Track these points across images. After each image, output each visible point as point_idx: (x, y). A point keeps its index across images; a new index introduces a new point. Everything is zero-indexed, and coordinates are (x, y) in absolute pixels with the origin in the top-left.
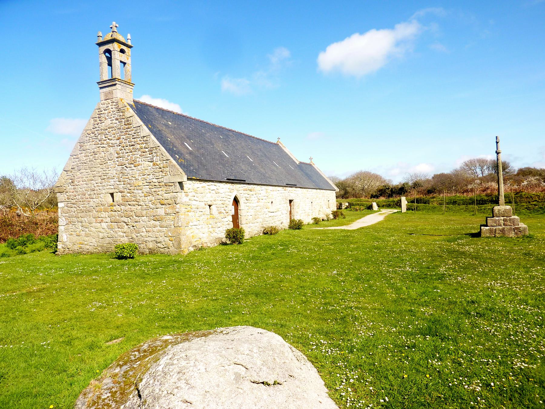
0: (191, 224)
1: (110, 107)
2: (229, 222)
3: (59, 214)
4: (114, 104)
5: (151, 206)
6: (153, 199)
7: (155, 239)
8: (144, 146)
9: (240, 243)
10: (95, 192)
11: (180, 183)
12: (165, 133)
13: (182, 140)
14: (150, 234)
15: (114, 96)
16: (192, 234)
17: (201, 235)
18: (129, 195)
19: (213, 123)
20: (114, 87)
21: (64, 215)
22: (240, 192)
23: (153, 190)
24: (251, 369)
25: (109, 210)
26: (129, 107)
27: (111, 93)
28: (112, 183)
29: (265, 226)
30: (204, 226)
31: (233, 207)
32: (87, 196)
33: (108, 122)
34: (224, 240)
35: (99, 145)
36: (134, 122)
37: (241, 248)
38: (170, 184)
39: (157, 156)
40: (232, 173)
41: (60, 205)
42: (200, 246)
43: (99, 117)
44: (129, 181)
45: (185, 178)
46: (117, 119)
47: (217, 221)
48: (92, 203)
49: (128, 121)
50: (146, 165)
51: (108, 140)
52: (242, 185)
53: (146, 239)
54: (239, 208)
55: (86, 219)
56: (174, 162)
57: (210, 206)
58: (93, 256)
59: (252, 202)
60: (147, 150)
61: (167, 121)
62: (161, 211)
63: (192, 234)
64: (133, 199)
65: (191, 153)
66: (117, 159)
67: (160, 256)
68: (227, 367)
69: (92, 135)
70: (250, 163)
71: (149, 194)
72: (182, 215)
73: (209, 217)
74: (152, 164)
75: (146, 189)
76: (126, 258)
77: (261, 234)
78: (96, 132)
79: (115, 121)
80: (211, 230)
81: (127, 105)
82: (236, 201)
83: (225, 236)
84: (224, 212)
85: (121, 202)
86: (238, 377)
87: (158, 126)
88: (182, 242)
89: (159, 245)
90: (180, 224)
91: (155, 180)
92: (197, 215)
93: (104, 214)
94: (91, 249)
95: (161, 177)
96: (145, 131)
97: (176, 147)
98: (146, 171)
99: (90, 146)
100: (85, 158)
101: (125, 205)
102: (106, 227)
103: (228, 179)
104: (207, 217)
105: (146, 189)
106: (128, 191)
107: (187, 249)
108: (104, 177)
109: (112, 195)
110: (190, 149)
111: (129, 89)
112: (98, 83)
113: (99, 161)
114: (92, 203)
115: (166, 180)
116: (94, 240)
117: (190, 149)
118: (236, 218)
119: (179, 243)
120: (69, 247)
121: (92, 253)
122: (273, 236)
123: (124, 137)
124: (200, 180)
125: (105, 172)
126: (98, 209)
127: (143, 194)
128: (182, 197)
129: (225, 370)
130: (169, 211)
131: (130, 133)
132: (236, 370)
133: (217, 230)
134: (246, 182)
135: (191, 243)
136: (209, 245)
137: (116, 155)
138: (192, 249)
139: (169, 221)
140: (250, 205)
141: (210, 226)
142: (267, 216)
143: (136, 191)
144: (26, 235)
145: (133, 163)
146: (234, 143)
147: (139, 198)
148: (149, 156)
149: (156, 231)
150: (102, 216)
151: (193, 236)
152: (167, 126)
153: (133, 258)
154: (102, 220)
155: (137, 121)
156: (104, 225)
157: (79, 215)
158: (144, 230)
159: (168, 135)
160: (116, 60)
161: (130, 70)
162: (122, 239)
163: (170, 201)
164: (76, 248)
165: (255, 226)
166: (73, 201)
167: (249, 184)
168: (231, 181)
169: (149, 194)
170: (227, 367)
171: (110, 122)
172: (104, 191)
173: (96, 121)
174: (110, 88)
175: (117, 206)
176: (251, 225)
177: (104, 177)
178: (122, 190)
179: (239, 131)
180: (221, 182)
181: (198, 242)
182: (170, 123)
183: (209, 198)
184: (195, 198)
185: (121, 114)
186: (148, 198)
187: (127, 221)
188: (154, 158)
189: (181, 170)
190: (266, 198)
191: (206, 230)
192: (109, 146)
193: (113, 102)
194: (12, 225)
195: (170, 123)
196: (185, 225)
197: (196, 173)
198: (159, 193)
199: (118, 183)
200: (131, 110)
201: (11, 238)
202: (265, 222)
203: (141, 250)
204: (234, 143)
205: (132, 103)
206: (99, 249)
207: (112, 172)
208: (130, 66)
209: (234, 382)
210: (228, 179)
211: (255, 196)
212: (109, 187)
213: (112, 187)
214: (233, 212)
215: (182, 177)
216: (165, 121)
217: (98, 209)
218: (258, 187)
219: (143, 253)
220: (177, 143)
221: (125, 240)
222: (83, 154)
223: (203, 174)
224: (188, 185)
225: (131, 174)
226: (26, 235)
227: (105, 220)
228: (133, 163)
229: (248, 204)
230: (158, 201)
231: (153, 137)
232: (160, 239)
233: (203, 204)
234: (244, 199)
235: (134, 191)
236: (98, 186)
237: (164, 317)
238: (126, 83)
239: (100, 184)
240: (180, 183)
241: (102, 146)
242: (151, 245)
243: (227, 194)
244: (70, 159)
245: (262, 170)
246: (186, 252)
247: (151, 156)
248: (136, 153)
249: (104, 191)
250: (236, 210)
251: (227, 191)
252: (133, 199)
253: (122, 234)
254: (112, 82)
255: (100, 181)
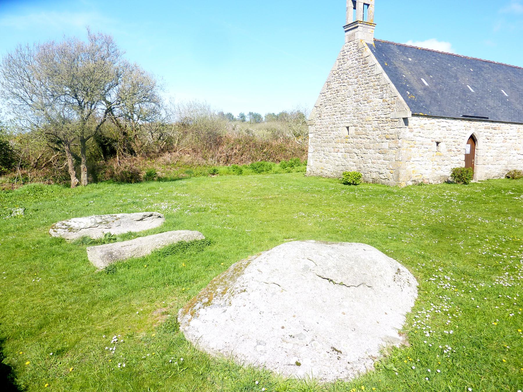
0: (413, 159)
1: (352, 49)
2: (460, 161)
3: (309, 143)
4: (356, 45)
5: (378, 140)
6: (380, 133)
7: (378, 170)
8: (376, 83)
9: (465, 183)
10: (335, 125)
11: (406, 120)
12: (402, 70)
13: (420, 75)
14: (375, 166)
15: (356, 38)
16: (413, 169)
17: (423, 171)
18: (360, 129)
19: (465, 55)
20: (356, 30)
21: (312, 144)
22: (480, 130)
23: (380, 125)
24: (319, 266)
25: (345, 141)
26: (367, 47)
27: (353, 35)
28: (349, 117)
29: (510, 169)
30: (427, 163)
31: (469, 145)
32: (329, 129)
33: (350, 62)
34: (450, 179)
35: (341, 84)
36: (370, 61)
37: (465, 189)
38: (396, 120)
39: (387, 93)
40: (472, 110)
41: (310, 136)
42: (420, 181)
43: (343, 59)
44: (362, 117)
45: (409, 114)
46: (357, 60)
47: (445, 159)
48: (332, 135)
49: (365, 60)
50: (376, 101)
51: (348, 79)
52: (483, 123)
53: (371, 169)
54: (476, 147)
55: (327, 148)
56: (401, 98)
57: (438, 143)
58: (330, 180)
59: (495, 141)
60: (379, 87)
61: (408, 57)
62: (385, 145)
63: (413, 169)
64: (364, 132)
65: (425, 89)
66: (354, 96)
67: (380, 186)
68: (301, 260)
69: (337, 75)
70: (502, 99)
71: (377, 128)
72: (404, 150)
73: (435, 154)
74: (382, 100)
75: (375, 124)
76: (349, 184)
77: (503, 178)
78: (340, 72)
79: (355, 61)
80: (436, 167)
81: (365, 45)
82: (473, 139)
83: (450, 174)
84: (455, 150)
85: (354, 135)
86: (306, 268)
87: (395, 63)
88: (400, 175)
89: (381, 176)
90: (400, 159)
91: (383, 116)
92: (421, 151)
93: (340, 145)
94: (329, 174)
95: (388, 113)
96: (379, 68)
97: (409, 83)
98: (376, 107)
99: (335, 85)
100: (330, 96)
101: (357, 138)
102: (340, 156)
103: (464, 116)
104: (432, 154)
105: (375, 124)
106: (361, 125)
107: (405, 182)
108: (343, 112)
109: (348, 128)
110: (426, 84)
111: (370, 29)
112: (344, 27)
113: (340, 98)
114: (332, 135)
115: (391, 116)
116: (331, 167)
117: (426, 84)
118: (470, 159)
119: (398, 176)
120: (314, 170)
121: (329, 178)
122: (514, 180)
123: (361, 75)
124: (428, 116)
125: (343, 108)
126: (336, 140)
127: (372, 129)
128: (405, 132)
129: (299, 261)
130: (392, 145)
131: (366, 71)
132: (307, 264)
133: (443, 168)
134: (489, 120)
135: (410, 177)
136: (431, 181)
137: (354, 92)
138: (410, 183)
139: (391, 154)
140: (492, 145)
141: (435, 163)
142: (515, 158)
143: (366, 126)
144: (295, 158)
145: (367, 100)
146: (487, 76)
147: (368, 132)
148: (380, 93)
149: (379, 163)
150: (339, 146)
151: (413, 171)
152: (406, 62)
153: (356, 185)
154: (338, 150)
155: (373, 60)
156: (340, 154)
157: (323, 144)
158: (370, 162)
159: (405, 72)
160: (360, 3)
161: (373, 11)
162: (352, 168)
163: (393, 136)
164: (318, 171)
165: (496, 168)
166: (319, 133)
167: (492, 122)
168: (467, 118)
169: (377, 128)
170: (301, 260)
171: (351, 62)
172: (342, 125)
173: (340, 62)
174: (351, 32)
175: (351, 139)
176: (490, 166)
177: (343, 112)
178: (356, 124)
179: (500, 62)
180: (455, 119)
181: (419, 178)
182: (410, 59)
183: (437, 135)
184: (421, 134)
185: (360, 54)
186: (376, 132)
187: (357, 152)
188: (384, 95)
189: (406, 106)
190: (516, 138)
191: (431, 167)
192: (349, 85)
193: (355, 44)
194: (286, 150)
195: (410, 59)
196: (406, 159)
197: (425, 109)
198: (385, 128)
199: (353, 118)
200: (369, 50)
201: (283, 160)
202: (511, 165)
203: (366, 179)
204: (487, 76)
205: (373, 43)
206: (335, 174)
207: (350, 108)
208: (373, 6)
209: (301, 270)
210: (464, 116)
211: (500, 135)
212: (346, 121)
213: (348, 121)
214: (468, 151)
215: (406, 114)
216: (405, 58)
217: (336, 140)
218: (507, 126)
219: (367, 182)
220: (413, 80)
221: (353, 169)
222: (329, 93)
223: (434, 110)
224: (413, 121)
225: (364, 110)
226: (295, 158)
227: (340, 150)
228: (367, 100)
229: (488, 144)
230: (384, 135)
231: (385, 75)
232: (382, 171)
233: (430, 140)
234: (484, 138)
235: (365, 126)
236: (338, 120)
237: (338, 232)
238: (368, 24)
239: (339, 119)
240: (406, 120)
241: (343, 84)
242: (374, 176)
243: (462, 131)
244: (320, 97)
245: (518, 106)
246: (403, 185)
247: (381, 93)
248: (369, 90)
249: (342, 125)
250: (473, 149)
251: (464, 129)
252: (364, 132)
253: (352, 163)
254: (353, 26)
255: (339, 116)
